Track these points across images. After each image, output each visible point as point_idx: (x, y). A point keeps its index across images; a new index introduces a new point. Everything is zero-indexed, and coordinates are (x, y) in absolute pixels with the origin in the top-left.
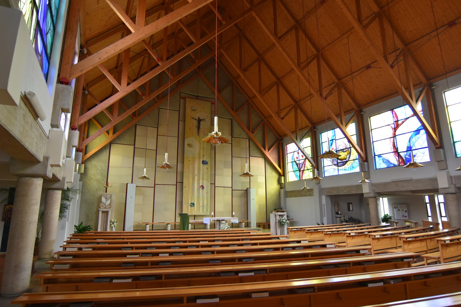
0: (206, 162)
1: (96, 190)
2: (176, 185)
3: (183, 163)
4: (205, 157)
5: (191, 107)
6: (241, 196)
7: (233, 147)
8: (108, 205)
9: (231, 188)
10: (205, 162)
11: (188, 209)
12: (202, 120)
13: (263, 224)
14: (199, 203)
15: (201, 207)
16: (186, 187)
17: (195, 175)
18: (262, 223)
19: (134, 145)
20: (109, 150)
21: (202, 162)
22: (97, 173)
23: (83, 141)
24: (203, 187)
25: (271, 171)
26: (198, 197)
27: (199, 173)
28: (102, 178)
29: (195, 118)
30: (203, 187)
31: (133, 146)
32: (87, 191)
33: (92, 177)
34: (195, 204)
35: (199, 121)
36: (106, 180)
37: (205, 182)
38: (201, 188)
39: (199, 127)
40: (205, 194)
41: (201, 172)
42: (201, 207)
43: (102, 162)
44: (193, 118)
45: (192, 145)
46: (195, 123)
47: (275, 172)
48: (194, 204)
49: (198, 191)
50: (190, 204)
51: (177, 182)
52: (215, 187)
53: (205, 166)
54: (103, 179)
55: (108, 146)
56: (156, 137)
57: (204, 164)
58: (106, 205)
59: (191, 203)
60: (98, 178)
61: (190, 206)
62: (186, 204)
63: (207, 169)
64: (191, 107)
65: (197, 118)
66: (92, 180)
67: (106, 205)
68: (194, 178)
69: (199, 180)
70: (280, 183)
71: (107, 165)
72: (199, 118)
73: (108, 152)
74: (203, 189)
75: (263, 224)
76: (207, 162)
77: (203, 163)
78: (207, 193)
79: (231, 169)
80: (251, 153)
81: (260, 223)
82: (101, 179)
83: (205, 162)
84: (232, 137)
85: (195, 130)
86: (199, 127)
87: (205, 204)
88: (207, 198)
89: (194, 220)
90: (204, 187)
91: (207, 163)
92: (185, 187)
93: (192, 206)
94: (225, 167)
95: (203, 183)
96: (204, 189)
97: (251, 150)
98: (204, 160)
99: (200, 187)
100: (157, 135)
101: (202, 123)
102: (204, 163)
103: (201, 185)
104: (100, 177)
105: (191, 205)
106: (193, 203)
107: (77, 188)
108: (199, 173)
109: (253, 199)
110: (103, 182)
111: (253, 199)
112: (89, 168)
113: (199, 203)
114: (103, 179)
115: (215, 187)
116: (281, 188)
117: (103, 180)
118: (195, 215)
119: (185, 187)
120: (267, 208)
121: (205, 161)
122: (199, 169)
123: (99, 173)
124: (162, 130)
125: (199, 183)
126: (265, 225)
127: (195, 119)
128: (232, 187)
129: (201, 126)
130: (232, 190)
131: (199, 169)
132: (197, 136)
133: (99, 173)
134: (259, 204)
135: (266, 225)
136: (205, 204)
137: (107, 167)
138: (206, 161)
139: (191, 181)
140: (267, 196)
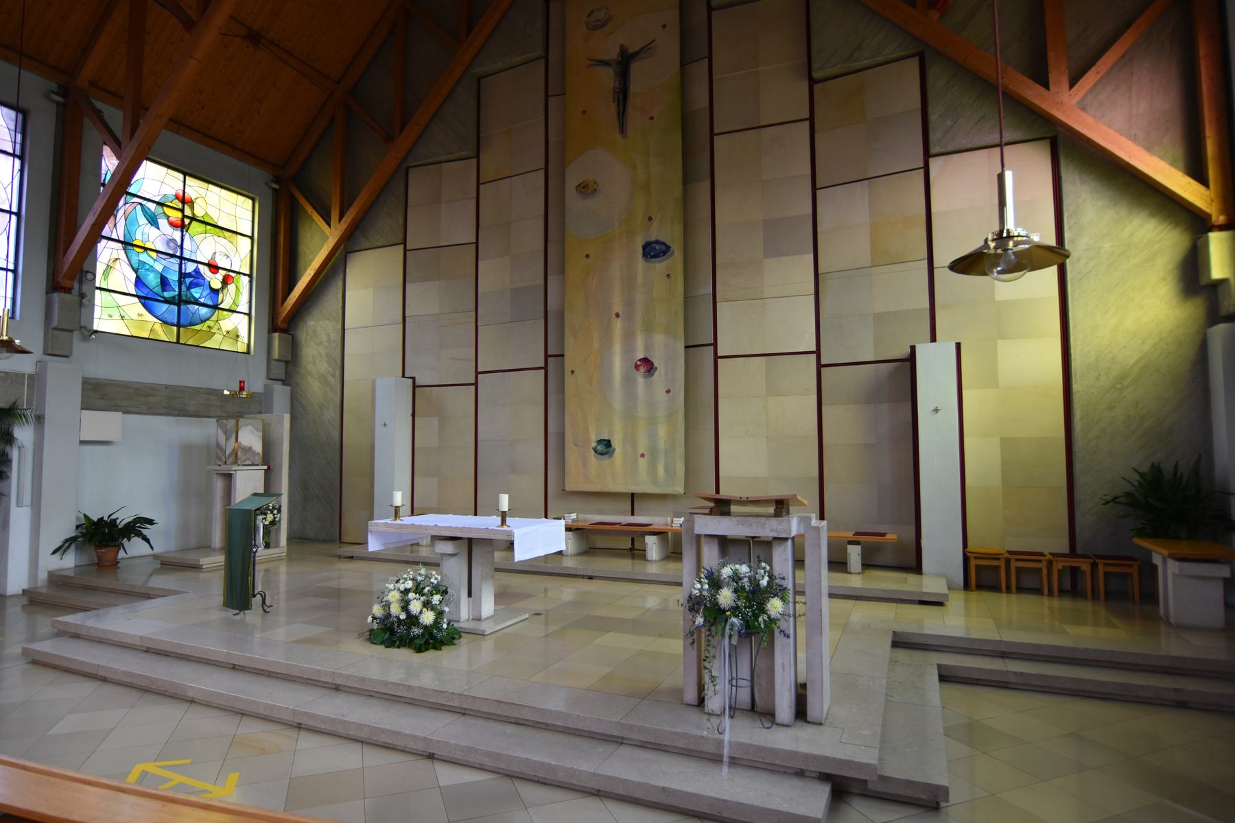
0: (663, 248)
1: (321, 408)
2: (546, 368)
3: (562, 271)
4: (655, 224)
5: (590, 15)
6: (872, 397)
7: (817, 136)
8: (230, 455)
9: (814, 356)
10: (658, 247)
11: (585, 464)
12: (636, 54)
13: (1014, 565)
14: (631, 440)
15: (642, 455)
16: (577, 372)
17: (614, 316)
18: (1008, 561)
19: (404, 243)
20: (341, 276)
21: (644, 248)
22: (320, 353)
23: (63, 257)
24: (647, 365)
25: (1110, 214)
26: (629, 414)
27: (629, 303)
28: (330, 369)
29: (605, 57)
30: (652, 364)
31: (402, 246)
32: (302, 411)
33: (308, 368)
34: (617, 444)
35: (625, 62)
36: (338, 373)
37: (659, 339)
38: (642, 369)
39: (622, 96)
40: (662, 397)
41: (639, 297)
42: (642, 455)
43: (328, 320)
44: (599, 61)
45: (595, 183)
46: (607, 78)
47: (1153, 215)
48: (608, 444)
49: (628, 382)
50: (594, 445)
51: (547, 356)
52: (716, 357)
53: (660, 266)
54: (332, 372)
55: (334, 268)
56: (474, 195)
57: (652, 257)
58: (227, 453)
59: (600, 442)
60: (323, 368)
61: (596, 451)
62: (576, 445)
63: (668, 276)
64: (590, 15)
65: (613, 54)
66: (309, 378)
67: (227, 453)
68: (607, 333)
69: (629, 336)
70: (1203, 282)
71: (339, 326)
72: (623, 50)
73: (340, 284)
74: (653, 375)
75: (1020, 564)
76: (668, 243)
77: (649, 253)
78: (668, 392)
79: (811, 256)
80: (934, 136)
81: (998, 559)
82: (329, 371)
83: (658, 247)
84: (812, 82)
85: (609, 111)
86: (622, 96)
87: (662, 444)
88: (671, 415)
89: (633, 514)
90: (656, 365)
91: (668, 248)
92: (573, 372)
93: (602, 454)
94: (774, 249)
95: (648, 347)
96: (656, 374)
97: (933, 117)
98: (653, 239)
99: (637, 367)
100: (478, 184)
101: (635, 68)
102: (654, 251)
103: (641, 355)
104: (326, 365)
105: (599, 448)
106: (606, 438)
107: (23, 405)
108: (629, 303)
109: (936, 410)
110: (332, 380)
111: (936, 410)
112: (303, 342)
113: (631, 440)
114: (332, 372)
115: (716, 357)
116: (1214, 316)
117: (334, 376)
118: (633, 495)
119: (573, 372)
120: (1078, 467)
121: (657, 242)
122: (629, 284)
123: (323, 353)
124: (492, 160)
125: (628, 349)
126: (997, 568)
127: (606, 63)
128: (818, 352)
129: (633, 89)
130: (820, 366)
131: (629, 284)
132: (618, 136)
133: (323, 353)
134: (1002, 439)
135: (1045, 571)
136: (662, 444)
137: (340, 334)
138: (660, 239)
139: (596, 346)
140: (1076, 386)
